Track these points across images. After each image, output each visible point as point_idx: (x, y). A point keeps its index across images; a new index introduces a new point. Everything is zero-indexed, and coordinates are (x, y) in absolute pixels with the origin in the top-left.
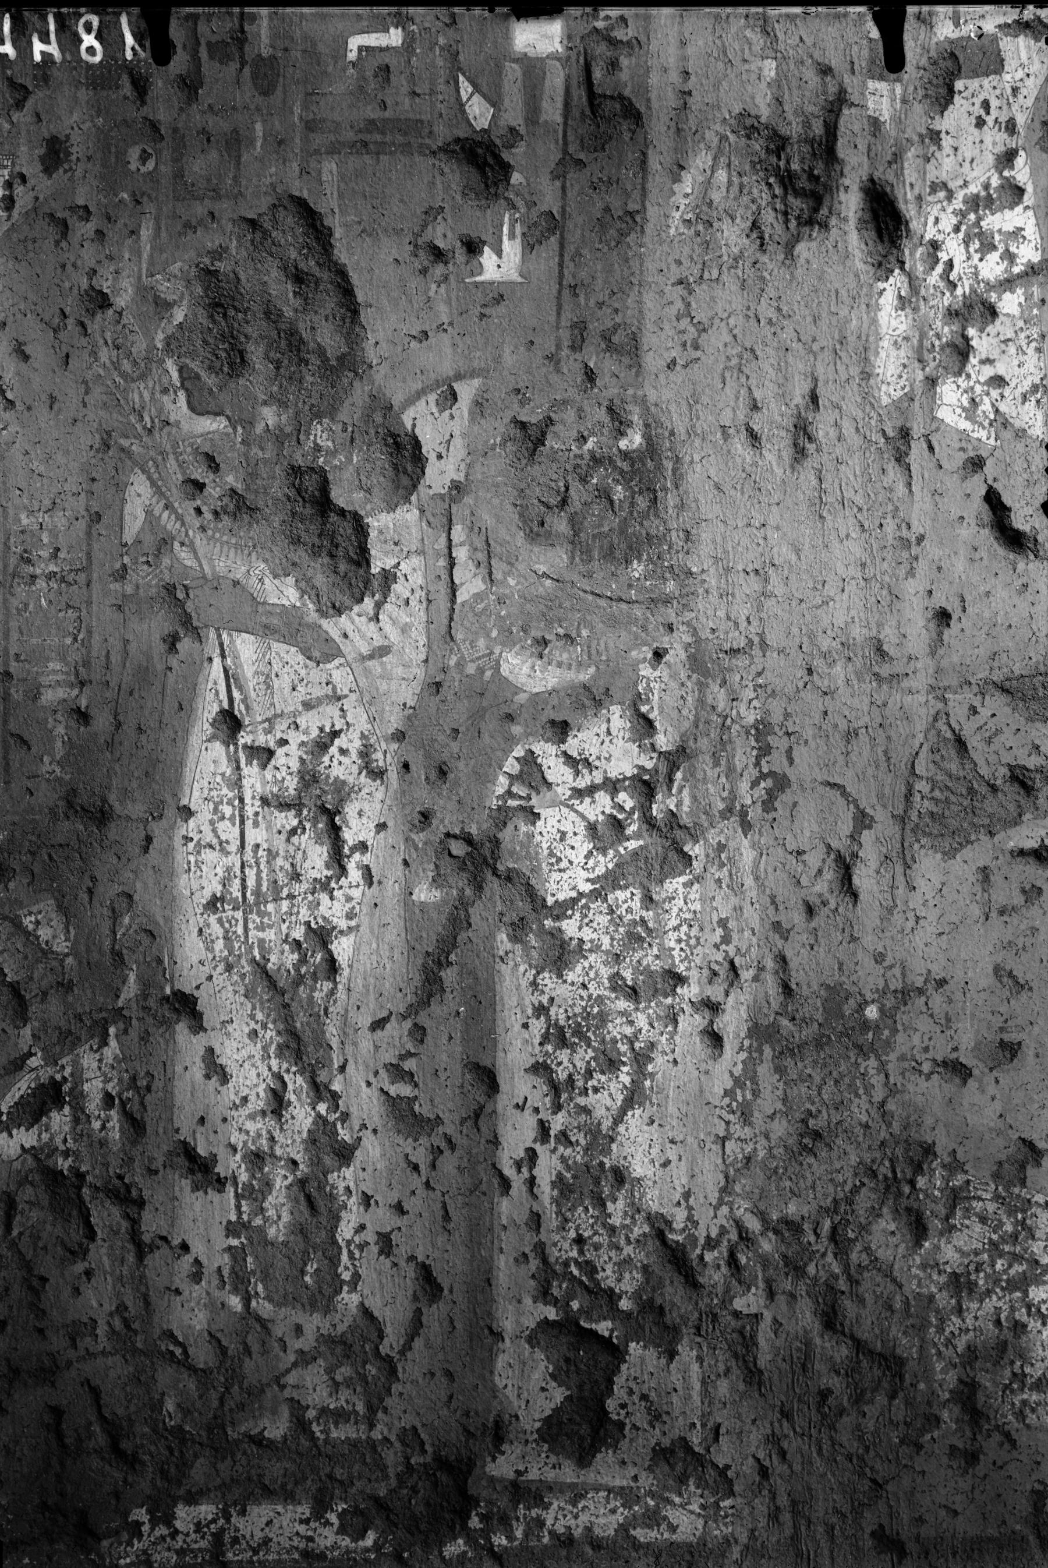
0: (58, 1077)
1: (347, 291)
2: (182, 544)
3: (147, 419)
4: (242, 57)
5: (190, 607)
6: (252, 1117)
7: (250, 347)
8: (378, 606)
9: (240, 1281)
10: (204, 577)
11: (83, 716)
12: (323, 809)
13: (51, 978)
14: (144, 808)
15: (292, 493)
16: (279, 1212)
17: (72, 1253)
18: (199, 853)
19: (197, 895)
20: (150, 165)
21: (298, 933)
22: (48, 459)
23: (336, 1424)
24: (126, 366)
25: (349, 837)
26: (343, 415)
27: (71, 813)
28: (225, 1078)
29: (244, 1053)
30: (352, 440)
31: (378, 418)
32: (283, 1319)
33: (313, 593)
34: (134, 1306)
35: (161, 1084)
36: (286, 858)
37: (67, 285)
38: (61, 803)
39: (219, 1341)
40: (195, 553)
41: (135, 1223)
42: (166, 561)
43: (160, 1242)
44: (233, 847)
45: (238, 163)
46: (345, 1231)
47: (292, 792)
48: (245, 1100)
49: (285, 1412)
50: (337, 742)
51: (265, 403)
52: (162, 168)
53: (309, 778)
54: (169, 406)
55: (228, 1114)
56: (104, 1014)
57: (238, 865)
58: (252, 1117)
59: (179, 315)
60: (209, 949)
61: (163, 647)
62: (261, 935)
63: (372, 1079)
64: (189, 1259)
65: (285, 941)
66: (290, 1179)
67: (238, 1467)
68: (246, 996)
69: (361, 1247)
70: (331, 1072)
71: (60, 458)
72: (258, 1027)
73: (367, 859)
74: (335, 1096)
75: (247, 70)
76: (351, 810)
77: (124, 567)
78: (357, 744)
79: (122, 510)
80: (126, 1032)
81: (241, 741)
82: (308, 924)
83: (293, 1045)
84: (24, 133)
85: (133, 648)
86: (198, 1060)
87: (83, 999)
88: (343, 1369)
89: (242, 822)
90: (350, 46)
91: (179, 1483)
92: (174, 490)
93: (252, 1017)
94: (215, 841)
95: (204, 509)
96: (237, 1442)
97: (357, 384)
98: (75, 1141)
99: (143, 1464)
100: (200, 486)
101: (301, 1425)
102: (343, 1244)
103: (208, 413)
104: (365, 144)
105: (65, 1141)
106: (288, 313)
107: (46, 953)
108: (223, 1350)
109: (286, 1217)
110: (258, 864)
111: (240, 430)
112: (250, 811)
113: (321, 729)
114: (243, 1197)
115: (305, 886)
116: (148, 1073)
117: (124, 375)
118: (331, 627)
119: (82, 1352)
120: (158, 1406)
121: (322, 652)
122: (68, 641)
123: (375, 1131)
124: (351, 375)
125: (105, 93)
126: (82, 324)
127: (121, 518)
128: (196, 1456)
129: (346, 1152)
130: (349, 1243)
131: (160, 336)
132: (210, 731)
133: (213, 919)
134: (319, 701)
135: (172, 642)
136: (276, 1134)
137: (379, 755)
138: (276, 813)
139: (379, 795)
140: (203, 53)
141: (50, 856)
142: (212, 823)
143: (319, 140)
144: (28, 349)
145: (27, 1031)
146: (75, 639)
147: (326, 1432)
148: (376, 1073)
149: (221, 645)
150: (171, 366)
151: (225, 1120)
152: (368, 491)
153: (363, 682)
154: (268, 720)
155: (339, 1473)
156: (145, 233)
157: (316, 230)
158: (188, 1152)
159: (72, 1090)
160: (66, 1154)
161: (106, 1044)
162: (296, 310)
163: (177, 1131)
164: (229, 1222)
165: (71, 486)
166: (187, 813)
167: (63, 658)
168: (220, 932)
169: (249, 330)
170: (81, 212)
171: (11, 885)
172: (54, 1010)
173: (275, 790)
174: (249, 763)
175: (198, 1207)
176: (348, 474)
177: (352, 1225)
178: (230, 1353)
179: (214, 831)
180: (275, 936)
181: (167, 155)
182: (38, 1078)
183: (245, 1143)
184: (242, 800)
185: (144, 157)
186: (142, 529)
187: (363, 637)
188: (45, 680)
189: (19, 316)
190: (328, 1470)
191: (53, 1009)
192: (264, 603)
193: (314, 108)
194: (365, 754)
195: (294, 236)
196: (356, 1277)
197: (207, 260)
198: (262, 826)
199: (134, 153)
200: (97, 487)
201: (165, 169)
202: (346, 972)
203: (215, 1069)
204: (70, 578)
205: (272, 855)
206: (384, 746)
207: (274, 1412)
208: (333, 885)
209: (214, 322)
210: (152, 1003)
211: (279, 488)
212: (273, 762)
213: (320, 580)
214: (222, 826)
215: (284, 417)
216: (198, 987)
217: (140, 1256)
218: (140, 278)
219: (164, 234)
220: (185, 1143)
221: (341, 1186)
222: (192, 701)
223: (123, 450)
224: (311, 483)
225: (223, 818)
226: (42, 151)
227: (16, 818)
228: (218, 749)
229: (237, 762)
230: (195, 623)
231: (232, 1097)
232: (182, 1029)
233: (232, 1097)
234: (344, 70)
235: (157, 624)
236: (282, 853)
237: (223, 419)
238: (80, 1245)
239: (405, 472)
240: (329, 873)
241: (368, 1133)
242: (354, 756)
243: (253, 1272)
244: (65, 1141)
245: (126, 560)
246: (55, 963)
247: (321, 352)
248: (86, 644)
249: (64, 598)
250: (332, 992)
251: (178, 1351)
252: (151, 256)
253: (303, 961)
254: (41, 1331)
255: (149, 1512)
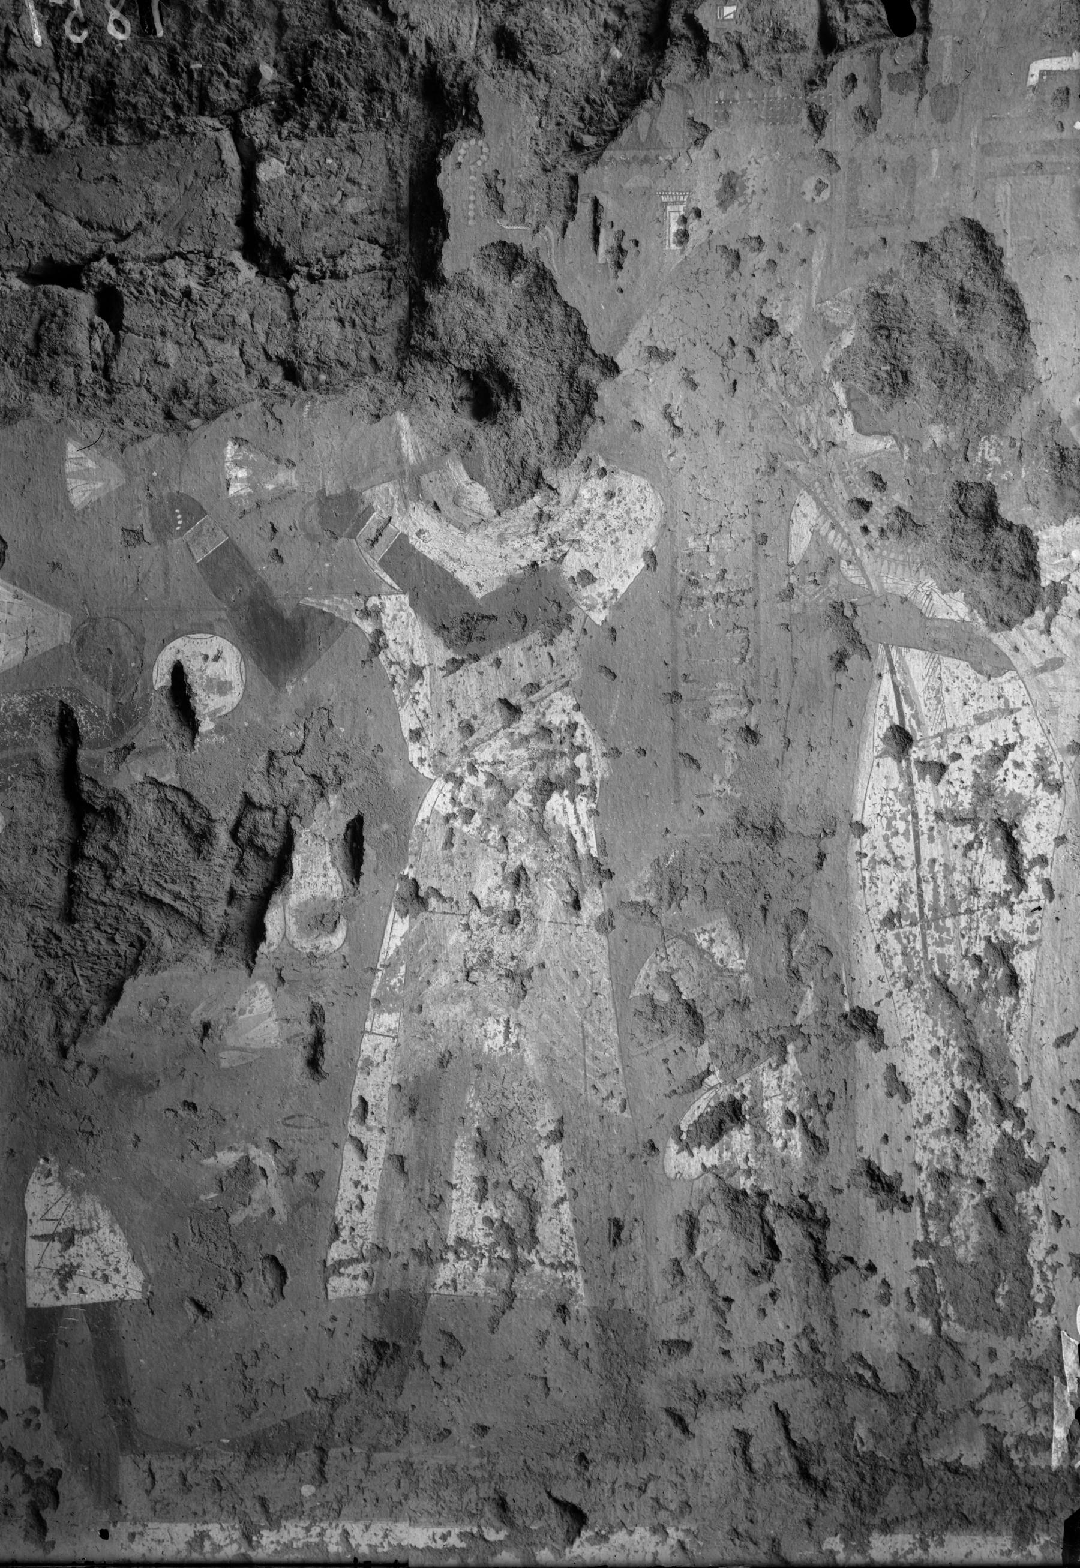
0: (737, 1095)
1: (1015, 308)
2: (849, 563)
3: (813, 441)
4: (922, 87)
5: (858, 624)
6: (936, 1135)
7: (914, 367)
8: (1049, 619)
9: (929, 1303)
10: (872, 594)
11: (751, 734)
12: (999, 823)
13: (727, 995)
14: (816, 825)
15: (955, 509)
16: (968, 1231)
17: (755, 1273)
18: (873, 869)
19: (874, 911)
20: (826, 194)
21: (979, 949)
22: (715, 482)
23: (1035, 1452)
24: (794, 390)
25: (1028, 850)
26: (1012, 431)
27: (741, 831)
28: (907, 1095)
29: (927, 1070)
30: (1020, 455)
31: (1046, 431)
32: (975, 1343)
33: (981, 607)
34: (822, 1331)
35: (842, 1102)
36: (963, 873)
37: (737, 314)
38: (732, 822)
39: (910, 1365)
40: (862, 569)
41: (818, 1244)
42: (833, 580)
43: (846, 1263)
44: (908, 863)
45: (913, 189)
46: (1036, 1252)
47: (967, 806)
48: (929, 1117)
49: (981, 1439)
50: (1011, 755)
51: (932, 422)
52: (837, 197)
53: (984, 792)
54: (836, 428)
55: (913, 1132)
56: (782, 1032)
57: (914, 880)
58: (936, 1135)
59: (847, 339)
60: (888, 965)
61: (830, 665)
62: (940, 950)
63: (1058, 1096)
64: (876, 1279)
65: (965, 956)
66: (978, 1198)
67: (934, 1495)
68: (927, 1013)
69: (1054, 1269)
70: (1015, 1088)
71: (727, 482)
72: (940, 1044)
73: (1047, 872)
74: (1020, 1114)
75: (926, 99)
76: (1028, 823)
77: (791, 587)
78: (1032, 757)
79: (788, 532)
80: (805, 1049)
81: (914, 756)
82: (988, 939)
83: (976, 1062)
84: (701, 169)
85: (800, 666)
86: (880, 1078)
87: (760, 1016)
88: (1040, 1395)
89: (917, 837)
90: (1032, 71)
91: (874, 1511)
92: (840, 510)
93: (934, 1033)
94: (889, 857)
95: (871, 527)
96: (933, 1470)
97: (1025, 399)
98: (757, 1159)
99: (835, 1490)
100: (866, 506)
101: (999, 1453)
102: (1035, 1266)
103: (875, 433)
104: (1040, 165)
105: (747, 1159)
106: (953, 332)
107: (722, 970)
108: (914, 1375)
109: (974, 1238)
110: (934, 878)
111: (906, 449)
112: (924, 826)
113: (995, 743)
114: (930, 1217)
115: (983, 901)
116: (829, 1091)
117: (791, 399)
118: (1001, 640)
119: (770, 1375)
120: (847, 1431)
121: (994, 665)
122: (736, 660)
123: (1063, 1149)
124: (1019, 390)
125: (783, 128)
126: (751, 352)
127: (788, 539)
128: (890, 1483)
129: (1032, 1171)
130: (1041, 1264)
131: (828, 360)
132: (881, 746)
133: (890, 935)
134: (992, 715)
135: (840, 661)
136: (962, 1152)
137: (1055, 768)
138: (952, 828)
139: (1057, 808)
140: (884, 87)
141: (722, 875)
142: (886, 838)
143: (995, 163)
144: (696, 378)
145: (705, 1049)
146: (743, 659)
147: (1025, 1460)
148: (1063, 1090)
149: (890, 661)
150: (838, 389)
151: (909, 1138)
152: (1036, 504)
153: (1036, 695)
154: (940, 735)
155: (1040, 1503)
156: (817, 261)
157: (986, 250)
158: (872, 1172)
159: (752, 1108)
160: (748, 1173)
161: (785, 1062)
162: (960, 330)
163: (861, 1149)
164: (917, 1243)
165: (737, 509)
166: (861, 829)
167: (731, 677)
168: (898, 948)
169: (913, 351)
170: (754, 244)
171: (684, 903)
172: (730, 1029)
173: (949, 804)
174: (922, 778)
175: (884, 1226)
176: (1017, 488)
177: (1043, 1246)
178: (922, 1377)
179: (888, 846)
180: (953, 952)
181: (842, 185)
182: (717, 1096)
183: (930, 1161)
184: (915, 815)
185: (820, 186)
186: (809, 549)
187: (1034, 650)
188: (713, 700)
189: (689, 346)
190: (1028, 1500)
191: (730, 1027)
192: (933, 619)
193: (991, 133)
194: (1041, 767)
195: (962, 259)
196: (1050, 1300)
197: (877, 285)
198: (938, 841)
199: (810, 185)
200: (763, 509)
201: (841, 198)
202: (1029, 988)
203: (899, 1087)
204: (736, 599)
205: (949, 870)
206: (1060, 759)
207: (970, 1439)
208: (1013, 899)
209: (877, 344)
210: (831, 1020)
211: (945, 505)
212: (946, 777)
213: (986, 594)
214: (895, 841)
215: (951, 435)
216: (878, 1004)
217: (825, 1277)
218: (809, 304)
219: (835, 260)
220: (868, 1163)
221: (1030, 1206)
222: (862, 717)
223: (789, 472)
224: (976, 500)
225: (897, 833)
226: (718, 186)
227: (688, 837)
228: (890, 763)
229: (910, 777)
230: (864, 640)
231: (916, 1115)
232: (862, 1045)
233: (916, 1115)
234: (1024, 94)
235: (827, 643)
236: (959, 868)
237: (890, 438)
238: (764, 1266)
239: (1071, 484)
240: (1009, 887)
241: (1057, 1150)
242: (1030, 769)
243: (943, 1294)
244: (747, 1159)
245: (793, 579)
246: (730, 981)
247: (989, 370)
248: (755, 664)
249: (732, 618)
250: (1015, 1008)
251: (868, 1375)
252: (822, 282)
253: (984, 975)
254: (726, 1353)
255: (843, 1540)
